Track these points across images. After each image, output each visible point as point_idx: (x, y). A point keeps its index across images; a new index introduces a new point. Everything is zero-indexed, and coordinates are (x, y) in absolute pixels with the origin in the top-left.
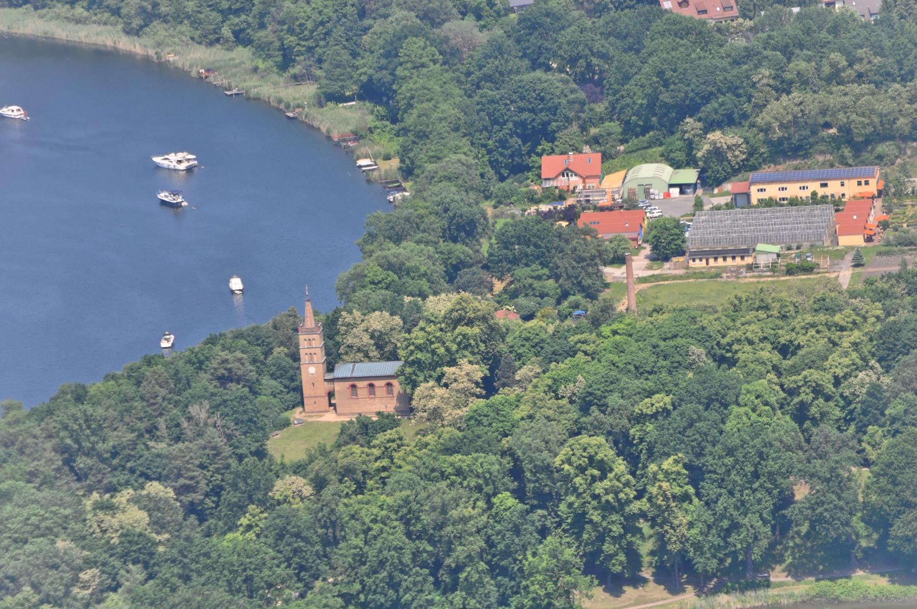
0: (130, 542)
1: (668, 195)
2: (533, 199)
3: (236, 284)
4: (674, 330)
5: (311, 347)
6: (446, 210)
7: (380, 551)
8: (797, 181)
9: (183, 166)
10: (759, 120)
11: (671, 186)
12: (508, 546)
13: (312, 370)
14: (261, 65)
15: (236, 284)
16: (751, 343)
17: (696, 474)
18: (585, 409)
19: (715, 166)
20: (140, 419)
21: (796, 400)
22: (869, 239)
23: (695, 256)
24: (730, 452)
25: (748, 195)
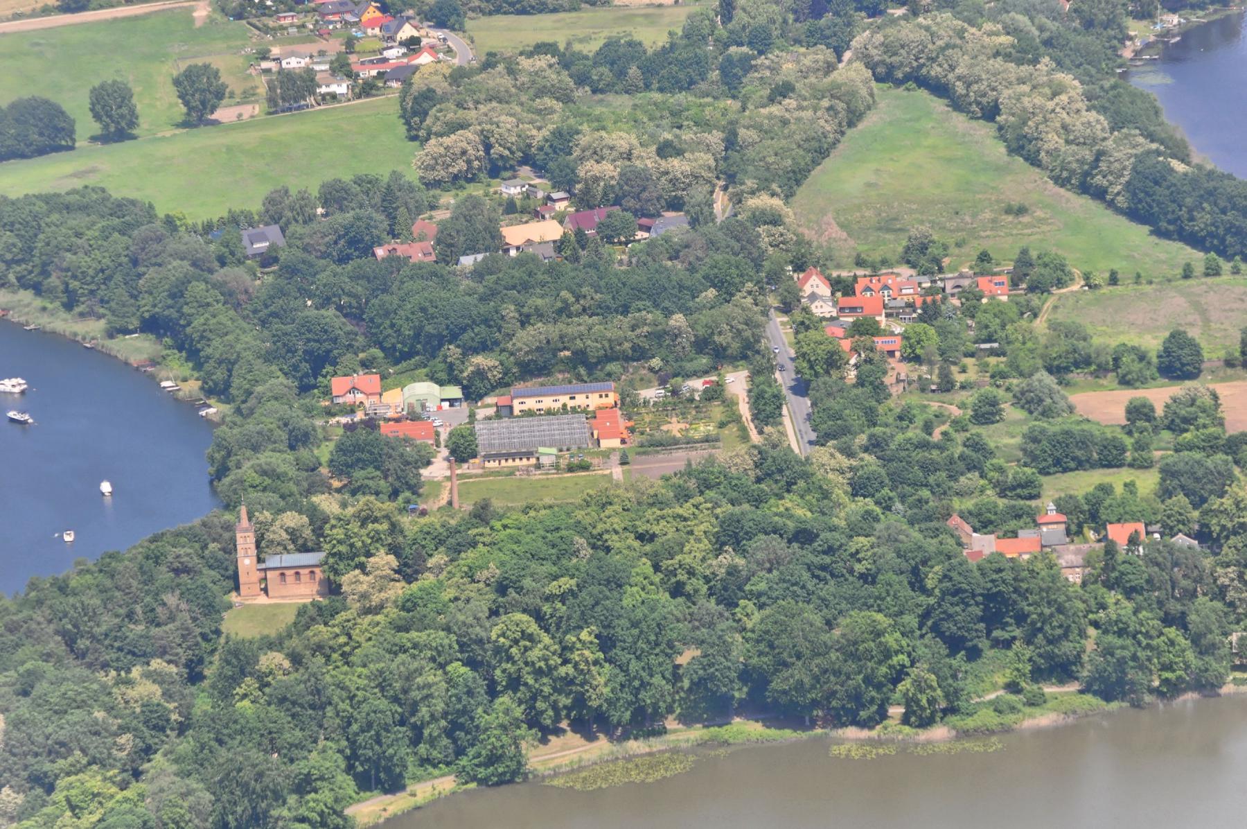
0: (151, 712)
1: (440, 408)
2: (330, 413)
3: (106, 487)
4: (556, 524)
5: (245, 542)
6: (286, 425)
7: (368, 714)
8: (552, 395)
9: (17, 390)
10: (509, 345)
11: (443, 400)
12: (465, 706)
13: (246, 561)
14: (49, 306)
15: (106, 487)
16: (616, 532)
17: (606, 643)
18: (502, 589)
19: (478, 383)
20: (120, 606)
21: (673, 580)
22: (623, 441)
23: (488, 457)
24: (635, 624)
25: (511, 408)
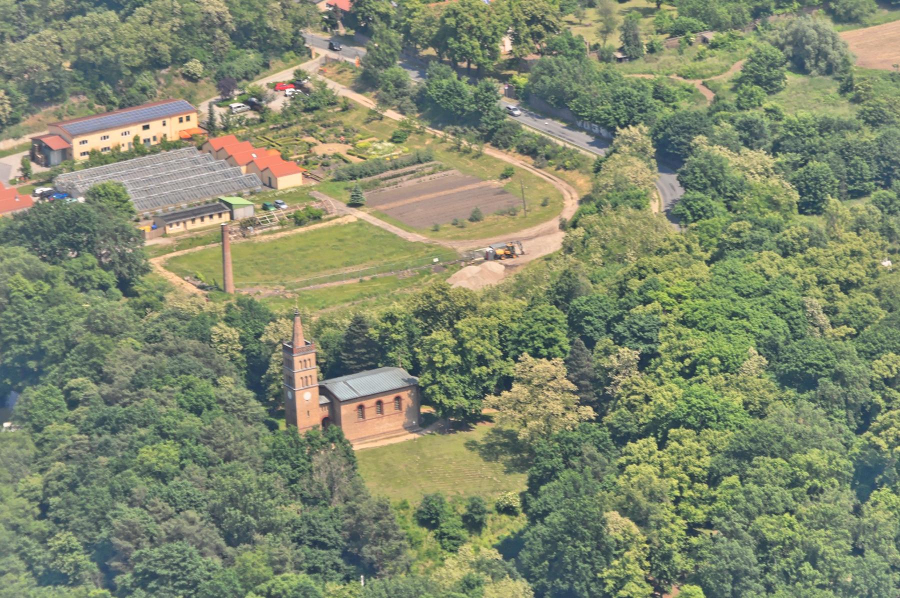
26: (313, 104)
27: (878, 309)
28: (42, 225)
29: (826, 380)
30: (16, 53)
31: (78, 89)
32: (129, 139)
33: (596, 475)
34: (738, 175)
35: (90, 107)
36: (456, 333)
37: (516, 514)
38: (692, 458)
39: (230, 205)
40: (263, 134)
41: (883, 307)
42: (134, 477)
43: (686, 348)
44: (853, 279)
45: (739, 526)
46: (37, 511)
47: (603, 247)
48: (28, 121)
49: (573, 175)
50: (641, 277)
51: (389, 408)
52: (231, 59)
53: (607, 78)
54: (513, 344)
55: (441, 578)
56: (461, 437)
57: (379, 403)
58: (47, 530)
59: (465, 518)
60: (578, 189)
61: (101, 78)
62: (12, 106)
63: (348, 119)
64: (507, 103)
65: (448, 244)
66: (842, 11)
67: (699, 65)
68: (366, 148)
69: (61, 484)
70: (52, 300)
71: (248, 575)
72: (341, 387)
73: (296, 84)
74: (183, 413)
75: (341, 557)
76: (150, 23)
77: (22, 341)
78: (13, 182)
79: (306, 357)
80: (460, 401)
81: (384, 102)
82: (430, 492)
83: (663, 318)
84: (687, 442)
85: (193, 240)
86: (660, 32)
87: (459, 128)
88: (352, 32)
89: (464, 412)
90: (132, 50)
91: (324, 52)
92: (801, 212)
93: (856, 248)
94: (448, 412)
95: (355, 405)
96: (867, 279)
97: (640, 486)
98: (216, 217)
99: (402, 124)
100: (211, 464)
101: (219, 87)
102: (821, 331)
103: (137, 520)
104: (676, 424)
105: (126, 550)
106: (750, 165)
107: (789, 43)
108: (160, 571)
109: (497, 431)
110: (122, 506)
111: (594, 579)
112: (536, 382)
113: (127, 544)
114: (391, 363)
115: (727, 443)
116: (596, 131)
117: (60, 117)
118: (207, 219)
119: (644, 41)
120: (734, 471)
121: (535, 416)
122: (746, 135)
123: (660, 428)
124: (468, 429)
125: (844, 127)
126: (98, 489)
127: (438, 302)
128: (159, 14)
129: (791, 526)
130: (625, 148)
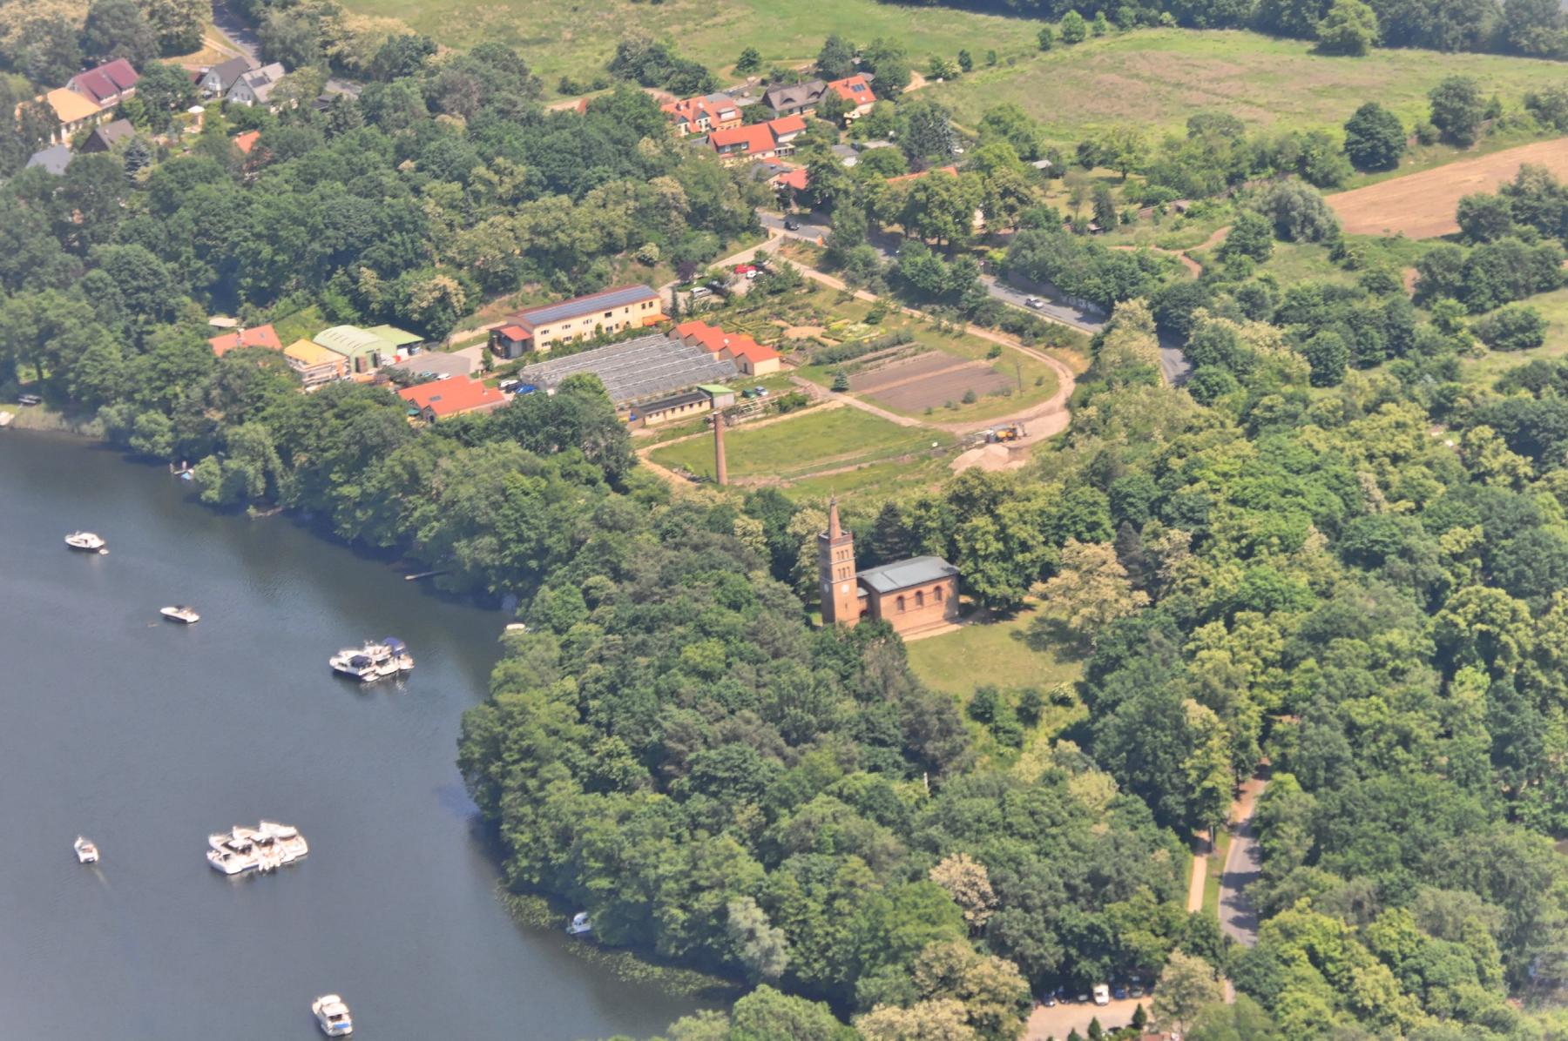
8: (582, 315)
11: (400, 347)
26: (779, 286)
27: (1433, 483)
28: (525, 418)
29: (1393, 557)
30: (468, 241)
31: (532, 277)
32: (592, 327)
33: (1164, 662)
34: (1248, 347)
35: (545, 295)
36: (997, 518)
37: (1072, 705)
38: (1264, 642)
39: (710, 394)
40: (730, 318)
41: (1437, 479)
42: (680, 677)
43: (1241, 528)
44: (1401, 451)
45: (1326, 710)
46: (577, 715)
47: (1126, 425)
48: (482, 312)
49: (1064, 353)
50: (1180, 457)
51: (929, 599)
52: (687, 242)
53: (1091, 251)
54: (1057, 530)
55: (1021, 773)
56: (1004, 627)
57: (919, 594)
58: (589, 734)
59: (1020, 711)
60: (1073, 367)
61: (555, 265)
62: (467, 296)
63: (817, 301)
64: (987, 280)
65: (945, 428)
66: (1319, 176)
67: (1178, 235)
68: (840, 331)
69: (599, 687)
70: (550, 497)
71: (817, 775)
72: (880, 578)
73: (757, 265)
74: (724, 610)
75: (901, 754)
76: (604, 206)
77: (521, 539)
78: (475, 375)
79: (843, 548)
80: (1002, 590)
81: (852, 282)
82: (983, 685)
83: (1212, 497)
84: (1258, 626)
85: (676, 432)
86: (1131, 201)
87: (937, 308)
88: (808, 211)
89: (1008, 601)
90: (587, 235)
91: (781, 233)
92: (1313, 385)
93: (1401, 420)
94: (992, 601)
95: (894, 597)
96: (1415, 452)
97: (1216, 672)
98: (696, 406)
99: (877, 304)
100: (758, 661)
101: (678, 271)
102: (1377, 507)
103: (690, 721)
104: (1242, 606)
105: (682, 752)
106: (1256, 336)
107: (1272, 210)
108: (720, 774)
109: (1041, 620)
110: (671, 708)
111: (1178, 770)
112: (1085, 567)
113: (681, 747)
114: (925, 552)
115: (1298, 626)
116: (1083, 306)
117: (515, 307)
118: (687, 409)
119: (1119, 211)
120: (1309, 654)
121: (1085, 603)
122: (1247, 306)
123: (1226, 610)
124: (1010, 618)
125: (1346, 295)
126: (643, 690)
127: (974, 487)
128: (614, 197)
129: (1378, 709)
130: (1125, 322)
